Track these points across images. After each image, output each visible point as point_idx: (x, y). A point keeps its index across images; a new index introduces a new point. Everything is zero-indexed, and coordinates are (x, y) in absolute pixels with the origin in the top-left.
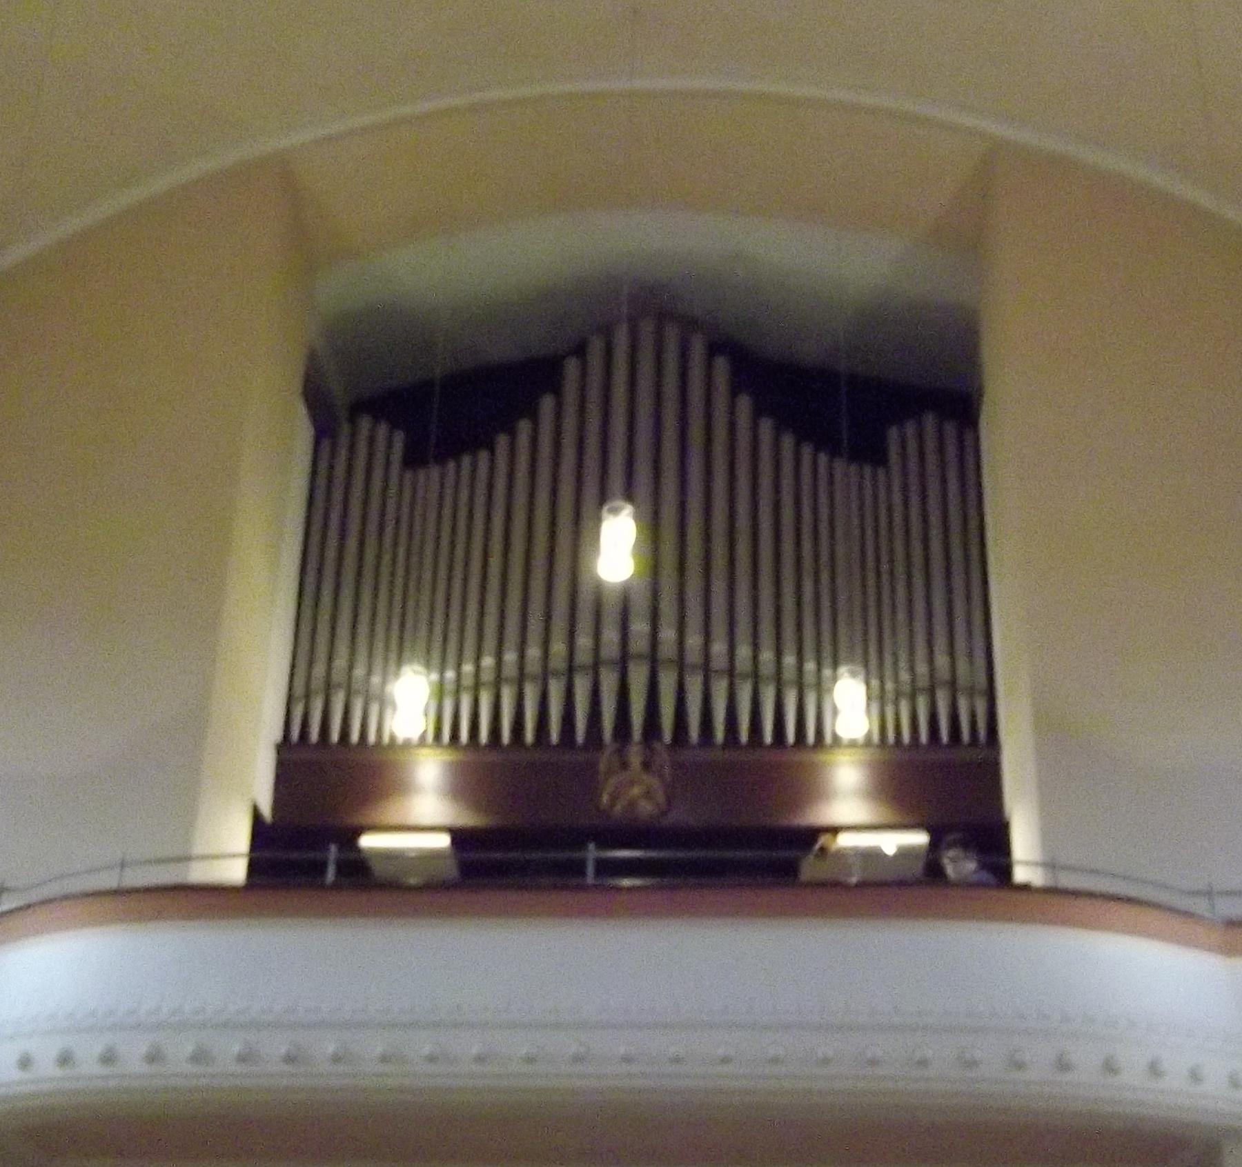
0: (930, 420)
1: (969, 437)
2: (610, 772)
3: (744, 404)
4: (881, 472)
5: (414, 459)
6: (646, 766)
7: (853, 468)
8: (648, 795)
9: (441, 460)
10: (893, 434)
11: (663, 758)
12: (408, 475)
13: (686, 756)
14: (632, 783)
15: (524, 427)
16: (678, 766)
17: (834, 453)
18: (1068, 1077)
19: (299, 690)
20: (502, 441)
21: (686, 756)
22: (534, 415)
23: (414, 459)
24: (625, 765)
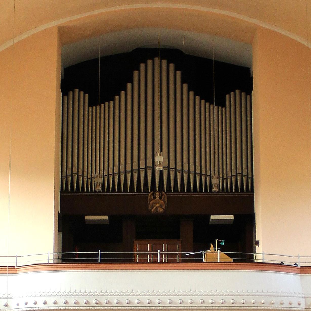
0: (77, 91)
1: (248, 96)
2: (151, 200)
3: (185, 86)
5: (93, 103)
6: (160, 198)
7: (216, 107)
8: (161, 206)
9: (103, 102)
10: (227, 96)
11: (165, 196)
12: (90, 108)
13: (171, 195)
14: (156, 203)
15: (123, 93)
17: (211, 103)
18: (292, 306)
19: (64, 175)
20: (117, 97)
21: (171, 195)
22: (125, 90)
23: (93, 103)
24: (155, 198)
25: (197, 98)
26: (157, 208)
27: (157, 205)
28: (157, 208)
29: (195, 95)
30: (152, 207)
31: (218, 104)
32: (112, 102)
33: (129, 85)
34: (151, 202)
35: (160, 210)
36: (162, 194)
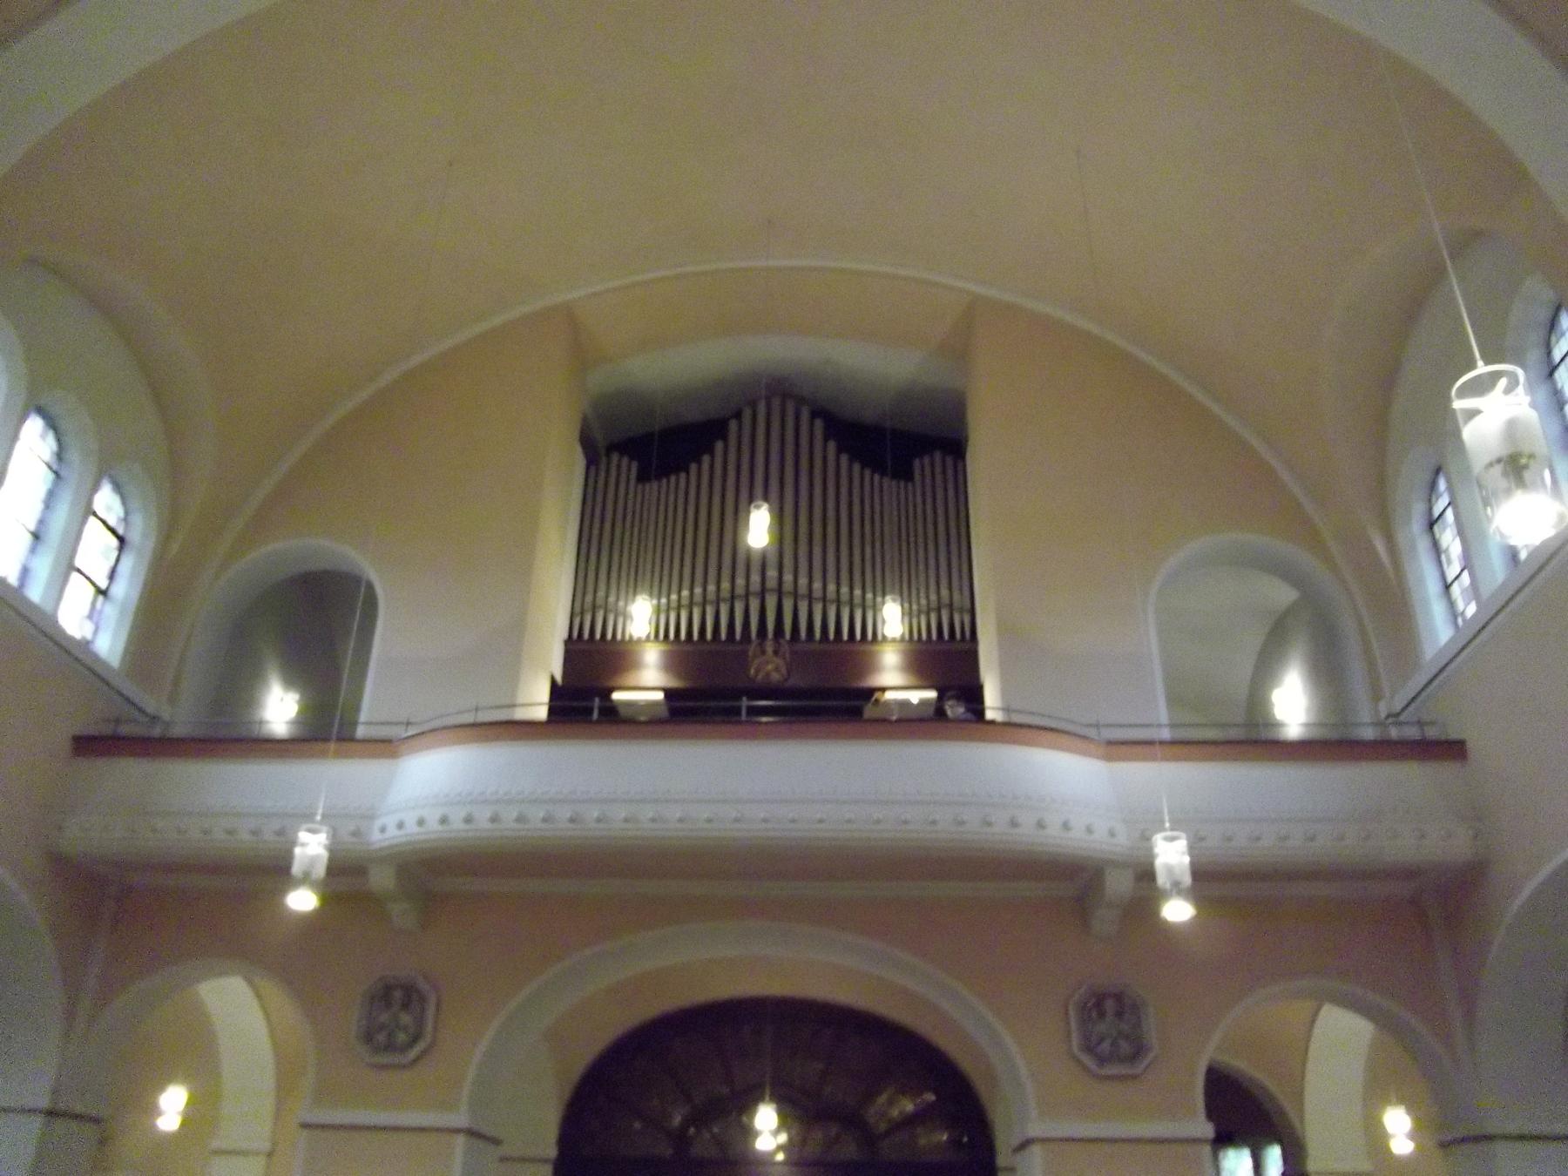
0: (938, 455)
1: (960, 468)
2: (755, 656)
3: (832, 446)
4: (910, 484)
5: (643, 477)
6: (776, 653)
7: (894, 483)
8: (777, 669)
9: (658, 478)
10: (917, 463)
11: (785, 648)
12: (640, 487)
13: (798, 647)
14: (768, 663)
16: (793, 653)
17: (883, 474)
19: (578, 609)
23: (643, 477)
24: (763, 652)
25: (844, 459)
26: (768, 674)
27: (770, 667)
28: (768, 674)
29: (839, 451)
30: (757, 671)
31: (896, 476)
32: (683, 475)
33: (719, 445)
34: (756, 662)
35: (776, 677)
36: (779, 644)
